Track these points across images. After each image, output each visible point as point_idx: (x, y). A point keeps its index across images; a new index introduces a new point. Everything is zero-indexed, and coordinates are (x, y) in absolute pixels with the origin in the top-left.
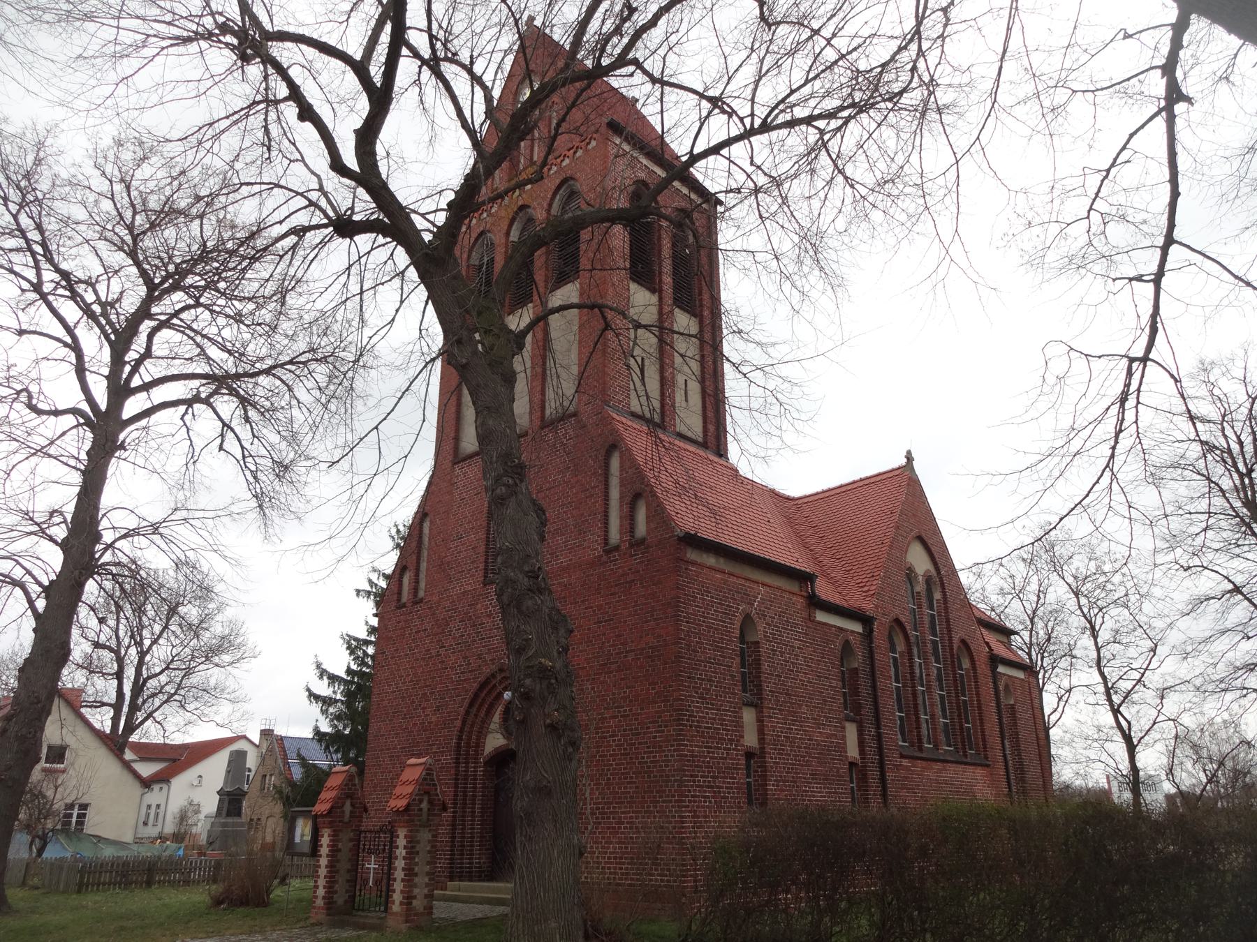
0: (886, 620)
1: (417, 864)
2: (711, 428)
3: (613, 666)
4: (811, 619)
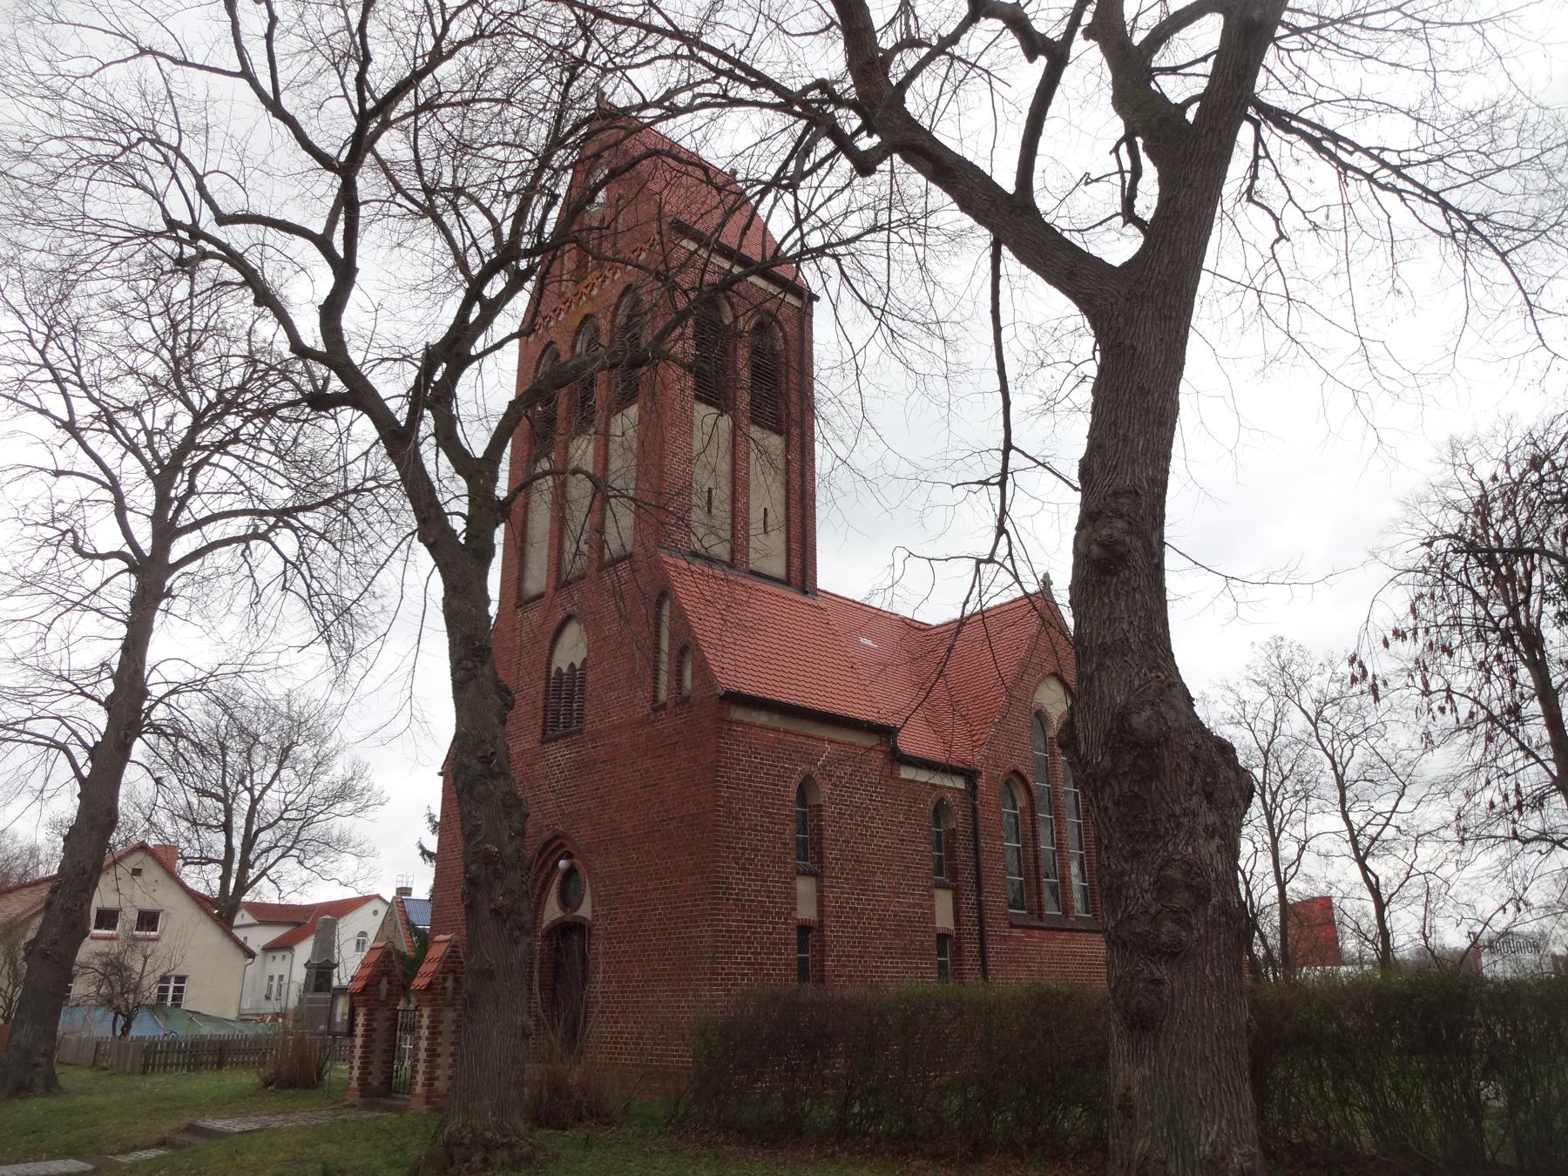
0: (999, 773)
1: (440, 1044)
2: (796, 561)
3: (658, 834)
4: (893, 776)
